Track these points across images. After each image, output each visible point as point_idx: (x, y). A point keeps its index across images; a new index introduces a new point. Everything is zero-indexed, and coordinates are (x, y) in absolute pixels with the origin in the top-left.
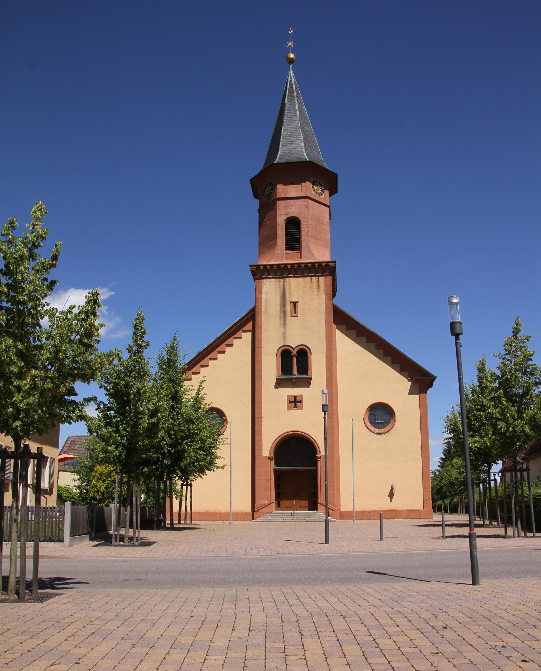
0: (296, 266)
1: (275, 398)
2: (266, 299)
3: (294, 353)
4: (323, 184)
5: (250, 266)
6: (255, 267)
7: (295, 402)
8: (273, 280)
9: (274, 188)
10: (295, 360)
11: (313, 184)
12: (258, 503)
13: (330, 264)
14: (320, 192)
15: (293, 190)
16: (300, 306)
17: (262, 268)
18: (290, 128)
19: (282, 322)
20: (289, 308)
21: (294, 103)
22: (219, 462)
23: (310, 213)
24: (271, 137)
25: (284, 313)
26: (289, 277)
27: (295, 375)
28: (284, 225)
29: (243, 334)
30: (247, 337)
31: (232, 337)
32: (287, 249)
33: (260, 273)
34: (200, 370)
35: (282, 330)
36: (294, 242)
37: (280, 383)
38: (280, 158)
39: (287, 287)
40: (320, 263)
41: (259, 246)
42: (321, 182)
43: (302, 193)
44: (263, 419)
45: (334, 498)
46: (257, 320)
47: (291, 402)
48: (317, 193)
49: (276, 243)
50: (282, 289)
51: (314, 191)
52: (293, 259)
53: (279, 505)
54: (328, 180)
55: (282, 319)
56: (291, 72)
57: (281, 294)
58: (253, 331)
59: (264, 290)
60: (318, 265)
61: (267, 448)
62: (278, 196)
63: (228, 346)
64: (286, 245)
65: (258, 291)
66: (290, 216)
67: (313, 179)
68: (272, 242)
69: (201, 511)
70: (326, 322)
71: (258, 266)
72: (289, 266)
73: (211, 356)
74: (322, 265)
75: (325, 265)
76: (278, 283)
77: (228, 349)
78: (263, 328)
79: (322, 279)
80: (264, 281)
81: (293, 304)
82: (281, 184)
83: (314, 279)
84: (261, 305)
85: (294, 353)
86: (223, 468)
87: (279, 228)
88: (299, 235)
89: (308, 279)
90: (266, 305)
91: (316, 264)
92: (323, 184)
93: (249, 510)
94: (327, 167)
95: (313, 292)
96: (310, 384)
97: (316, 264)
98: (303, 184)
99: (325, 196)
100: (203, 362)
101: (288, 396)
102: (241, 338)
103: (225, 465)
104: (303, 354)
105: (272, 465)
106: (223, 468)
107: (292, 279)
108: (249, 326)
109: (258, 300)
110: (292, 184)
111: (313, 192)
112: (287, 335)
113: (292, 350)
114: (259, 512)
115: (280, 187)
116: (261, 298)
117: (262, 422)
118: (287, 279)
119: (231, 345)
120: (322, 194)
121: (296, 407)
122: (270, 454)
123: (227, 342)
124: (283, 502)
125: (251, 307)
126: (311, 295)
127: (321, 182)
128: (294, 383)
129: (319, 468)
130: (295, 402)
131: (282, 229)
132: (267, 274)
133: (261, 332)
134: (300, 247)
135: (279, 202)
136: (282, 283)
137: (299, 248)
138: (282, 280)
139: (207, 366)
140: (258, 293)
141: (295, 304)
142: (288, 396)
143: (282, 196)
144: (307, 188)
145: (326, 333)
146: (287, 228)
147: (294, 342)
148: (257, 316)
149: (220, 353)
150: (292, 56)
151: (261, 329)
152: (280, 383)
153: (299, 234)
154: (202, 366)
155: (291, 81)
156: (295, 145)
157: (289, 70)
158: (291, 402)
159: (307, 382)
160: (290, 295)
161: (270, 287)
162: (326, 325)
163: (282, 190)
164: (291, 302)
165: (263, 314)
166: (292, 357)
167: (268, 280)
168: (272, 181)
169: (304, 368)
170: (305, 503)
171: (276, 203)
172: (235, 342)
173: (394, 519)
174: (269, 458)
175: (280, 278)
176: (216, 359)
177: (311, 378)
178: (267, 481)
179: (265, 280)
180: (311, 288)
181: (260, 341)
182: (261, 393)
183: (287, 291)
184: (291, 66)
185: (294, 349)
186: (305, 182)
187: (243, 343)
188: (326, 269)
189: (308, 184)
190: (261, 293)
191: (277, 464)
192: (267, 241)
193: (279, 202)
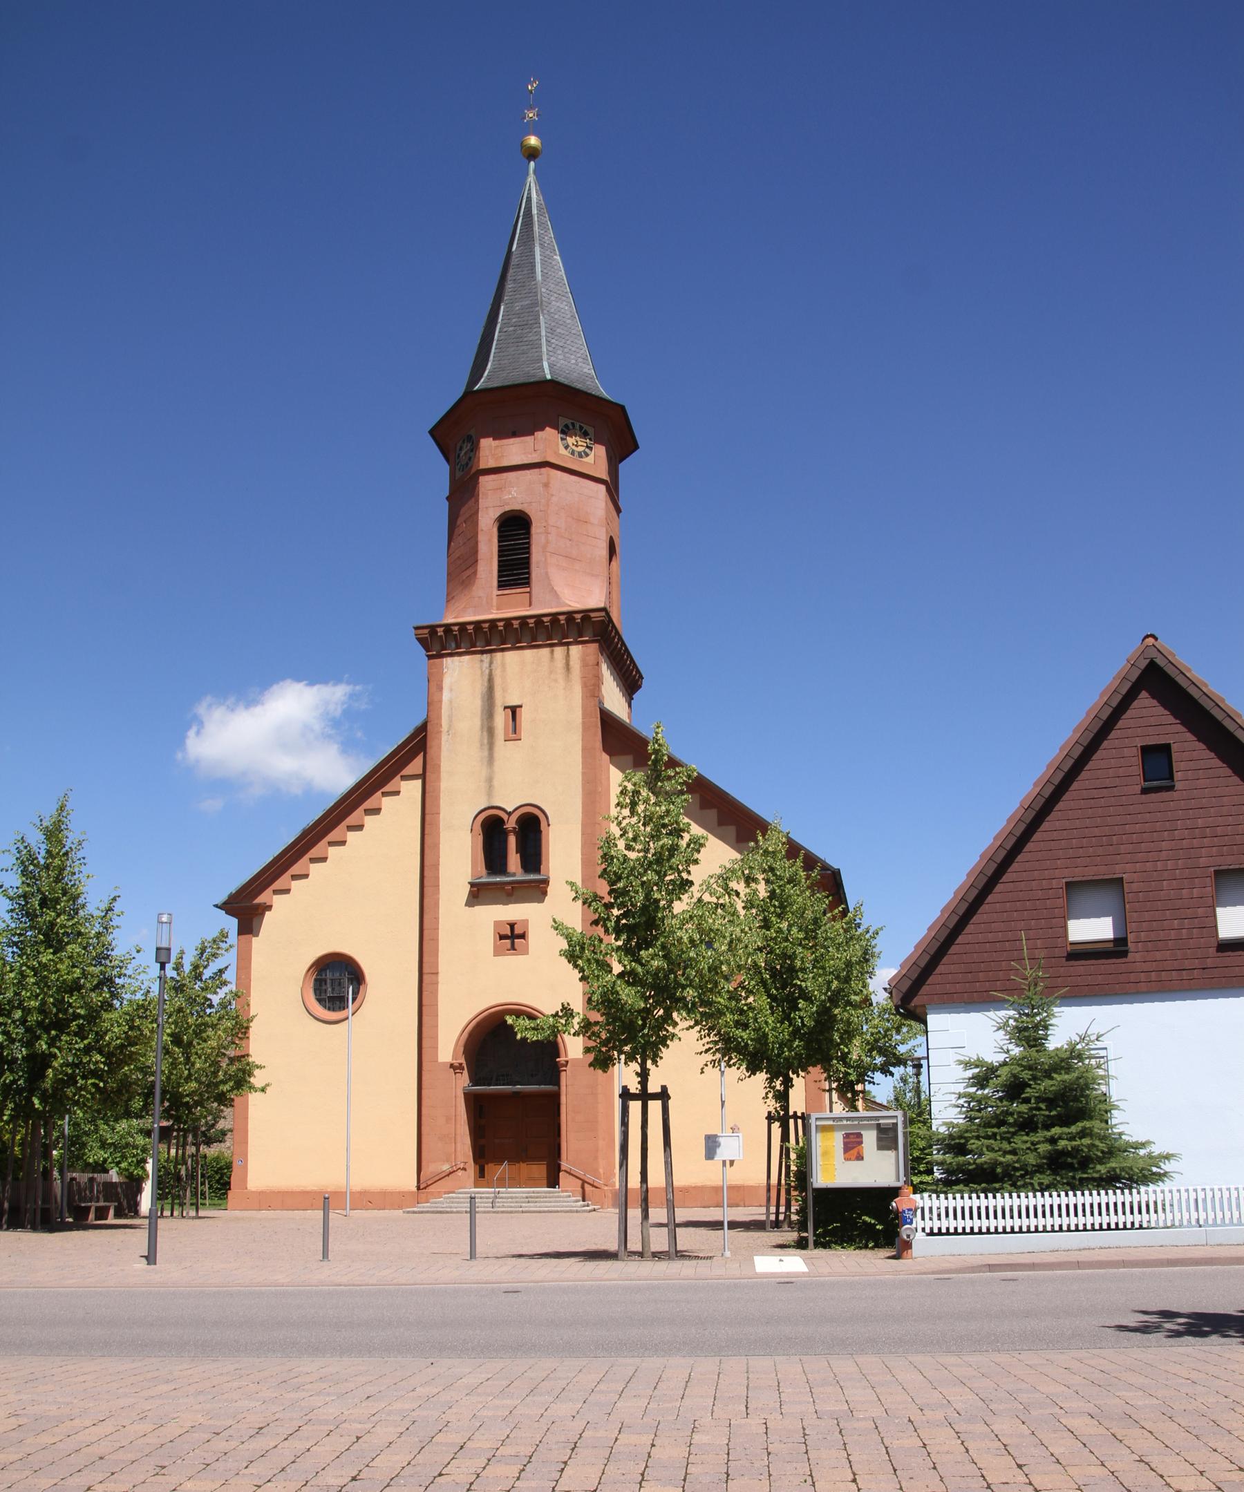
0: (516, 624)
1: (468, 928)
2: (451, 702)
3: (511, 824)
4: (591, 430)
5: (416, 628)
6: (426, 631)
7: (512, 937)
8: (466, 658)
9: (475, 448)
10: (512, 840)
11: (563, 432)
12: (430, 1169)
13: (592, 615)
14: (581, 449)
15: (515, 450)
16: (525, 716)
17: (440, 631)
18: (517, 306)
19: (486, 753)
20: (501, 719)
21: (532, 251)
22: (257, 1079)
23: (554, 499)
24: (482, 330)
25: (491, 731)
26: (503, 650)
27: (514, 875)
28: (495, 530)
29: (403, 783)
30: (411, 789)
31: (379, 793)
32: (502, 585)
33: (441, 641)
34: (308, 869)
35: (484, 773)
36: (515, 569)
37: (478, 894)
38: (489, 378)
39: (497, 674)
40: (570, 615)
41: (448, 582)
42: (585, 427)
43: (534, 455)
44: (441, 978)
45: (596, 1158)
46: (431, 752)
47: (502, 937)
48: (573, 453)
49: (475, 573)
50: (486, 678)
51: (567, 447)
52: (513, 607)
53: (481, 1173)
54: (610, 426)
55: (486, 747)
56: (531, 179)
57: (485, 690)
58: (423, 777)
59: (447, 682)
60: (567, 620)
61: (448, 1046)
62: (482, 466)
63: (369, 812)
64: (499, 576)
65: (434, 683)
66: (507, 508)
67: (563, 421)
68: (468, 572)
69: (309, 1189)
70: (584, 749)
71: (433, 629)
72: (501, 624)
73: (331, 836)
74: (574, 619)
75: (582, 619)
76: (478, 665)
77: (369, 820)
78: (443, 769)
79: (575, 650)
80: (448, 661)
81: (509, 711)
82: (488, 436)
83: (559, 651)
84: (440, 718)
85: (511, 824)
86: (263, 1090)
87: (482, 538)
88: (528, 553)
89: (545, 652)
90: (450, 717)
91: (561, 617)
92: (591, 430)
93: (412, 1184)
94: (604, 394)
95: (556, 681)
96: (545, 893)
97: (561, 617)
98: (539, 434)
99: (596, 459)
100: (314, 852)
101: (497, 924)
102: (397, 793)
103: (268, 1085)
104: (531, 826)
105: (464, 1080)
106: (263, 1090)
107: (509, 654)
108: (415, 766)
109: (432, 704)
110: (514, 434)
111: (563, 451)
112: (495, 783)
113: (505, 817)
114: (430, 1189)
115: (487, 444)
116: (441, 701)
117: (437, 983)
118: (499, 655)
119: (377, 811)
120: (587, 455)
121: (513, 948)
122: (454, 1057)
123: (368, 804)
124: (489, 1167)
125: (418, 722)
126: (552, 689)
127: (585, 427)
128: (513, 893)
129: (563, 1088)
130: (512, 937)
131: (490, 540)
132: (453, 645)
133: (438, 779)
134: (528, 578)
135: (483, 480)
136: (486, 665)
137: (526, 582)
138: (486, 657)
139: (324, 859)
140: (433, 689)
141: (514, 710)
142: (497, 924)
143: (492, 464)
144: (549, 443)
145: (584, 774)
146: (501, 538)
147: (510, 800)
148: (431, 743)
149: (351, 828)
150: (533, 141)
151: (439, 772)
152: (478, 894)
153: (527, 549)
154: (313, 860)
155: (529, 199)
156: (562, 351)
157: (527, 174)
158: (502, 937)
159: (537, 890)
160: (505, 690)
161: (461, 675)
162: (584, 757)
163: (491, 451)
164: (506, 708)
165: (444, 738)
166: (505, 833)
167: (456, 658)
168: (472, 432)
169: (533, 857)
170: (540, 1170)
171: (477, 483)
172: (387, 803)
173: (738, 1206)
174: (452, 1066)
175: (482, 652)
176: (343, 843)
177: (546, 882)
178: (448, 1119)
179: (449, 660)
180: (551, 672)
181: (438, 798)
182: (437, 919)
183: (498, 682)
184: (532, 164)
185: (509, 814)
186: (543, 429)
187: (400, 807)
188: (595, 629)
189: (549, 434)
190: (440, 688)
191: (475, 1080)
192: (461, 569)
193: (483, 480)
